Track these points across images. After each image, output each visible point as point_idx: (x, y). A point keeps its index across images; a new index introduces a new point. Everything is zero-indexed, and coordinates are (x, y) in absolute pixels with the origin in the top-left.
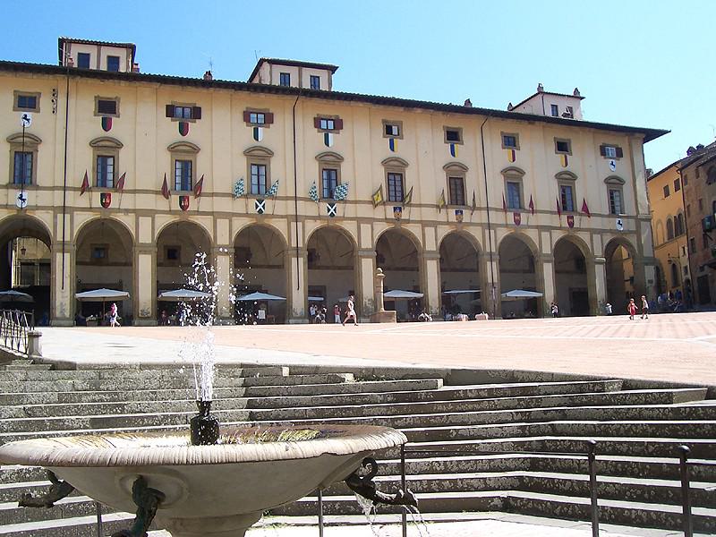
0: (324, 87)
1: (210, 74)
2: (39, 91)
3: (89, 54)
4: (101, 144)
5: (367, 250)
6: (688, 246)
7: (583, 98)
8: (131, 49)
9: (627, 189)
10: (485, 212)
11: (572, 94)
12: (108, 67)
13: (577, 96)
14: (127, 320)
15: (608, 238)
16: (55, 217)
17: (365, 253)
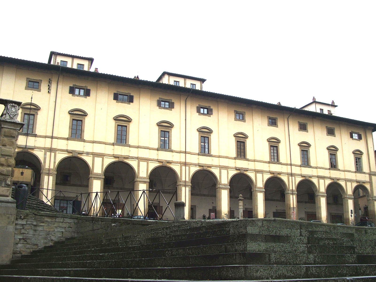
2: (41, 79)
4: (168, 125)
5: (224, 185)
7: (336, 106)
8: (91, 60)
9: (364, 158)
15: (355, 185)
16: (45, 154)
17: (100, 177)
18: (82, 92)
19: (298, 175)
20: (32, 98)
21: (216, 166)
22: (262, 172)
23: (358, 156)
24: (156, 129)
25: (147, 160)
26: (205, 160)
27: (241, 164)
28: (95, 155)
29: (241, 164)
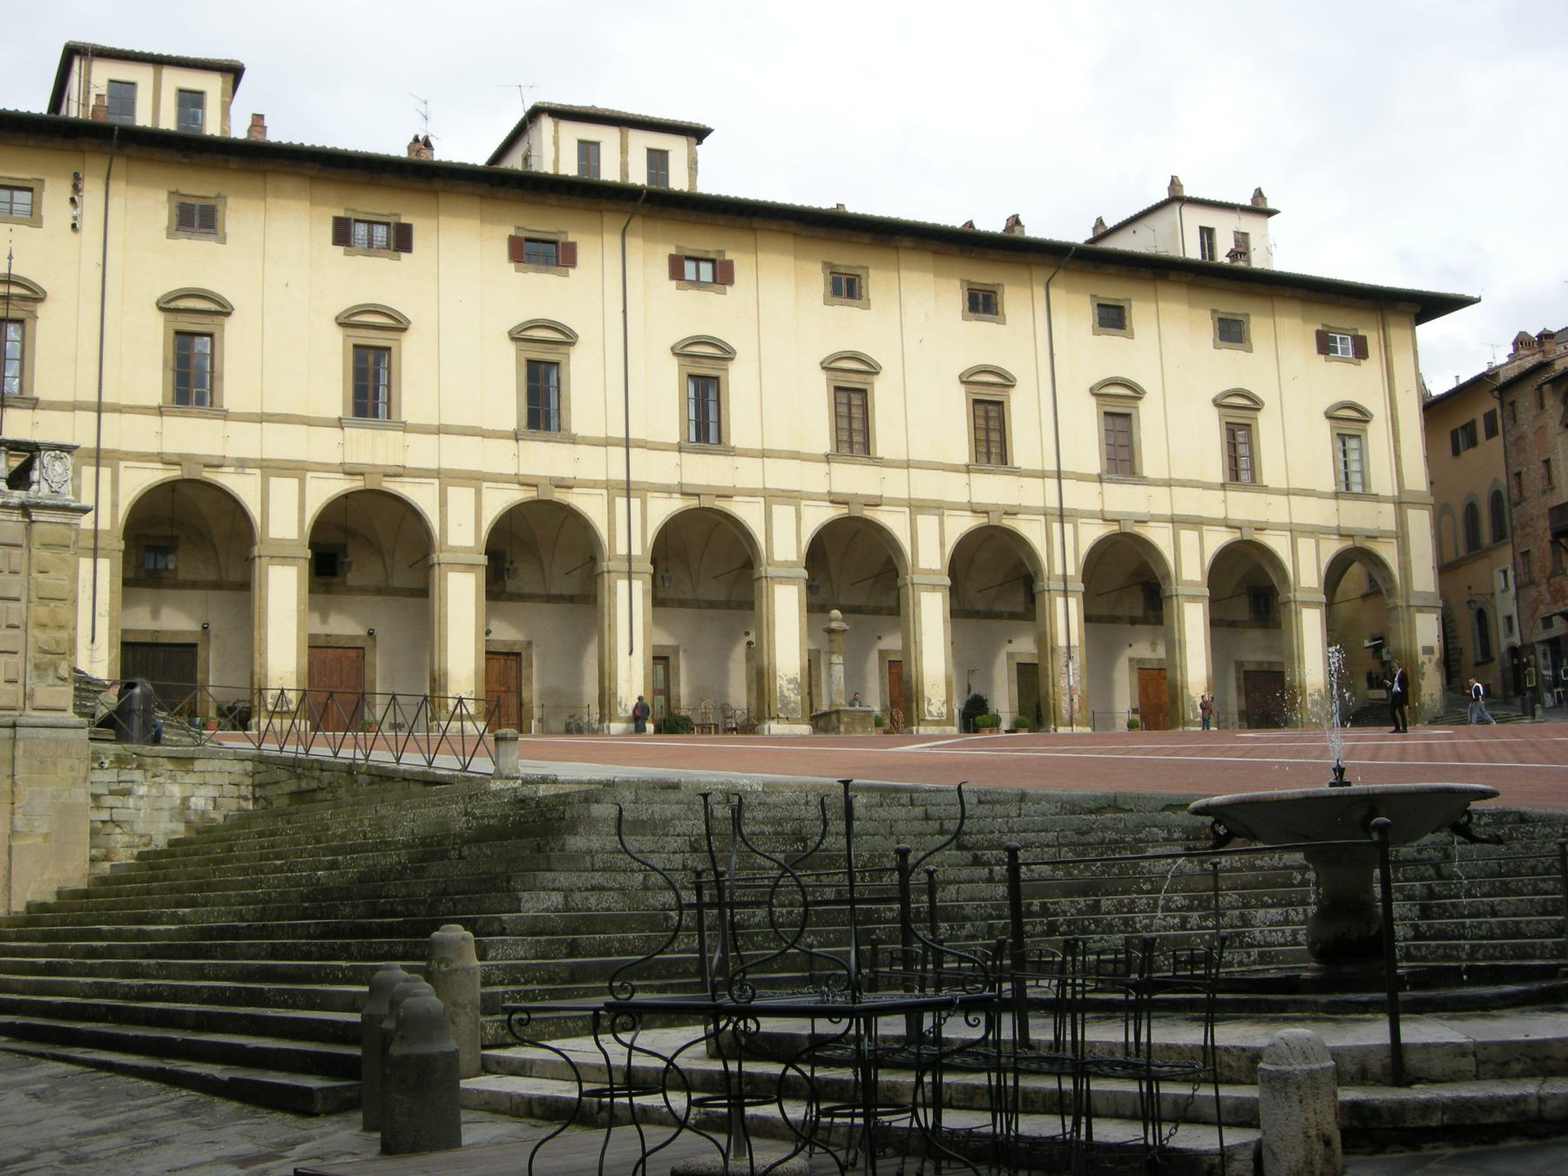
0: (678, 181)
1: (427, 144)
3: (202, 93)
4: (213, 307)
6: (1515, 569)
7: (1270, 213)
9: (1377, 434)
10: (1052, 483)
11: (1249, 203)
12: (580, 166)
13: (1259, 209)
14: (717, 732)
15: (1332, 547)
16: (77, 474)
18: (706, 271)
19: (1091, 515)
20: (10, 257)
21: (751, 493)
22: (937, 508)
23: (1238, 417)
24: (1324, 429)
25: (474, 479)
26: (706, 471)
27: (854, 479)
28: (270, 468)
29: (854, 479)
